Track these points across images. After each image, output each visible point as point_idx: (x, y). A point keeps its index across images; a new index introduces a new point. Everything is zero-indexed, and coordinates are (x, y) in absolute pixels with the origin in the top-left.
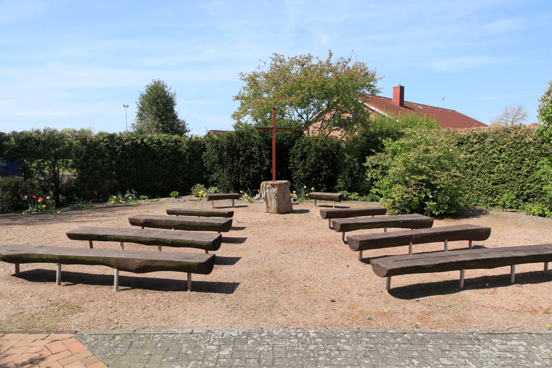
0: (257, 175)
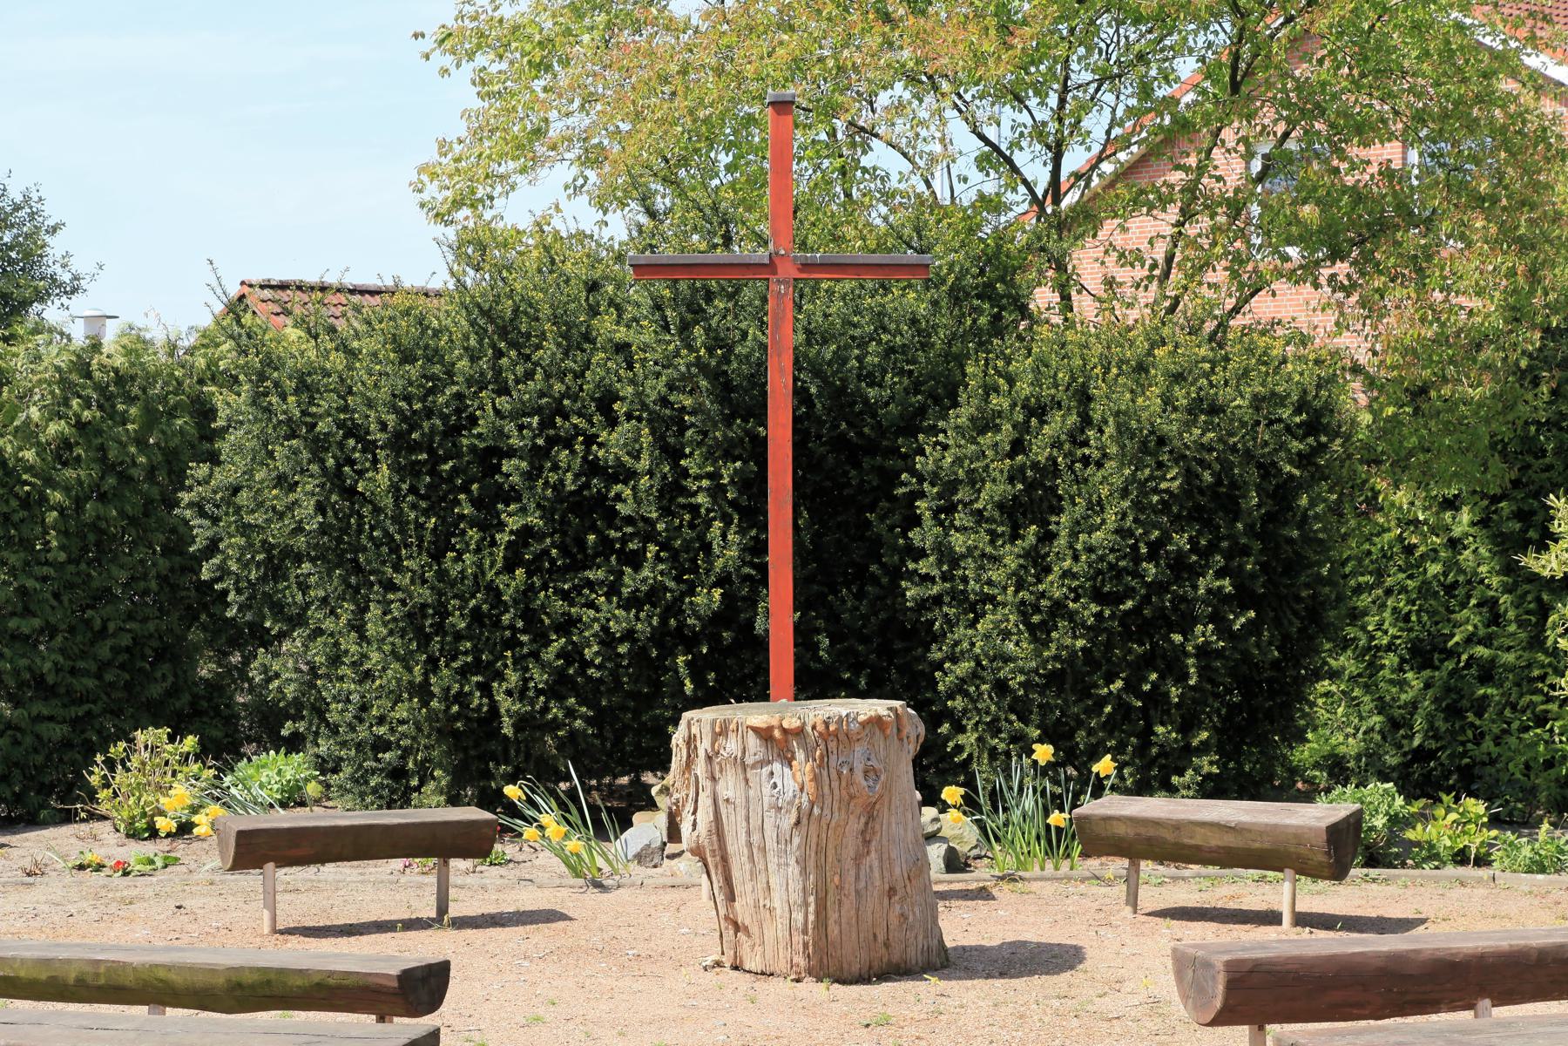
0: (639, 655)
